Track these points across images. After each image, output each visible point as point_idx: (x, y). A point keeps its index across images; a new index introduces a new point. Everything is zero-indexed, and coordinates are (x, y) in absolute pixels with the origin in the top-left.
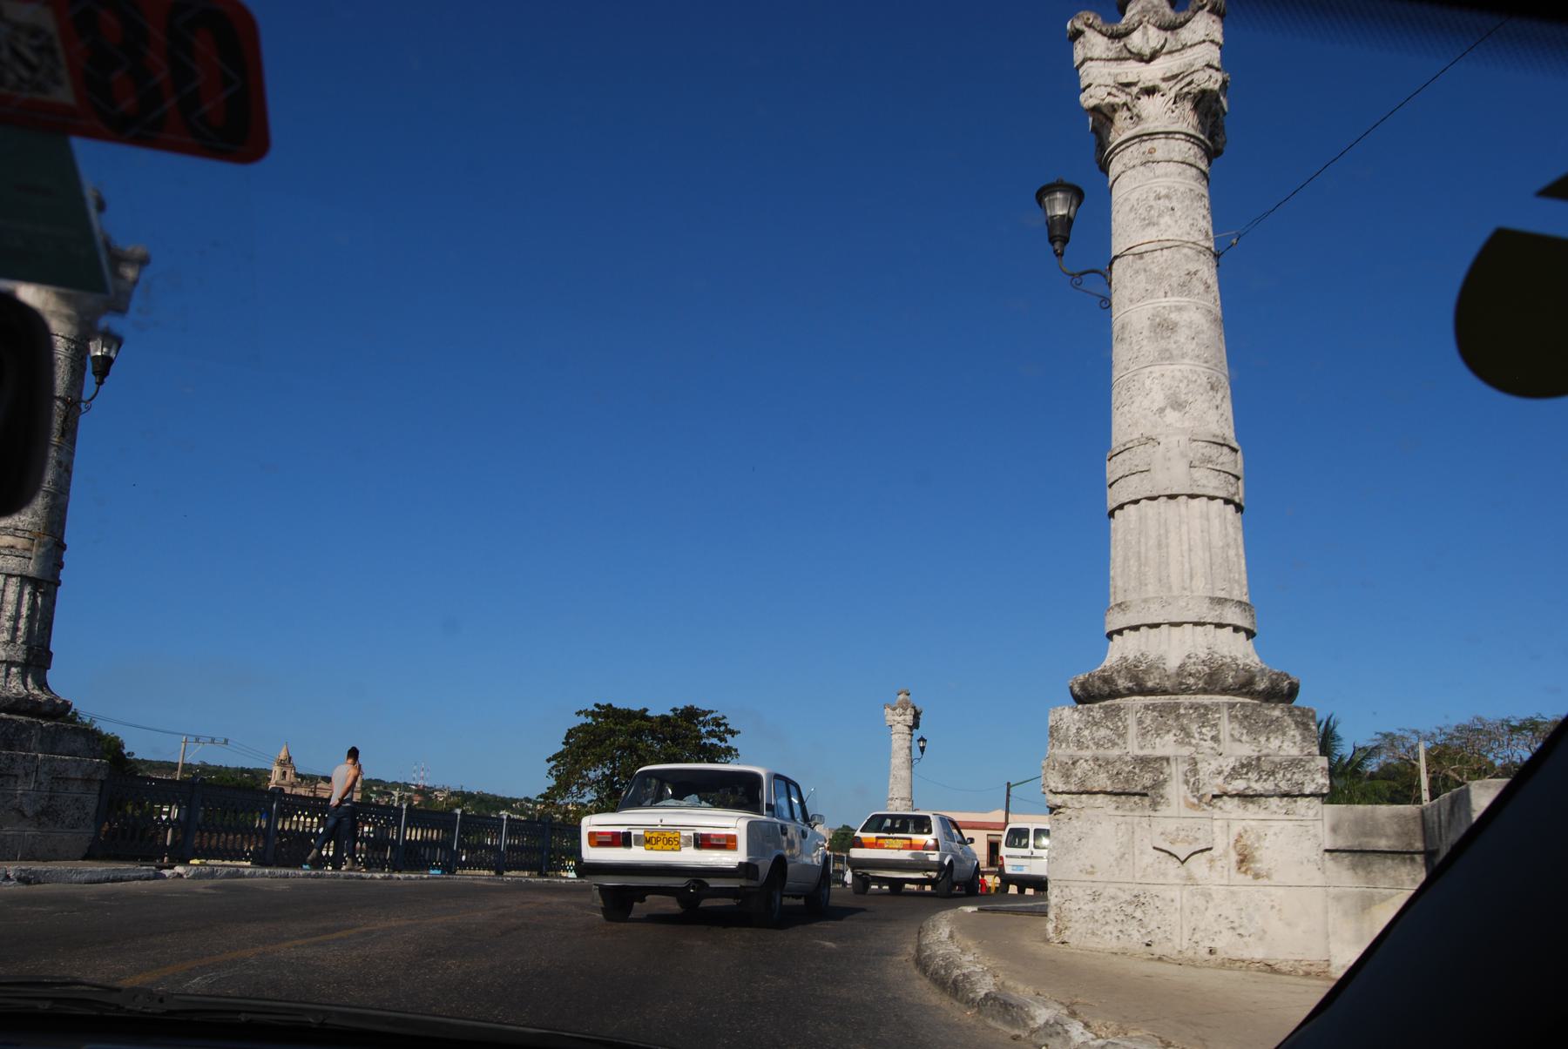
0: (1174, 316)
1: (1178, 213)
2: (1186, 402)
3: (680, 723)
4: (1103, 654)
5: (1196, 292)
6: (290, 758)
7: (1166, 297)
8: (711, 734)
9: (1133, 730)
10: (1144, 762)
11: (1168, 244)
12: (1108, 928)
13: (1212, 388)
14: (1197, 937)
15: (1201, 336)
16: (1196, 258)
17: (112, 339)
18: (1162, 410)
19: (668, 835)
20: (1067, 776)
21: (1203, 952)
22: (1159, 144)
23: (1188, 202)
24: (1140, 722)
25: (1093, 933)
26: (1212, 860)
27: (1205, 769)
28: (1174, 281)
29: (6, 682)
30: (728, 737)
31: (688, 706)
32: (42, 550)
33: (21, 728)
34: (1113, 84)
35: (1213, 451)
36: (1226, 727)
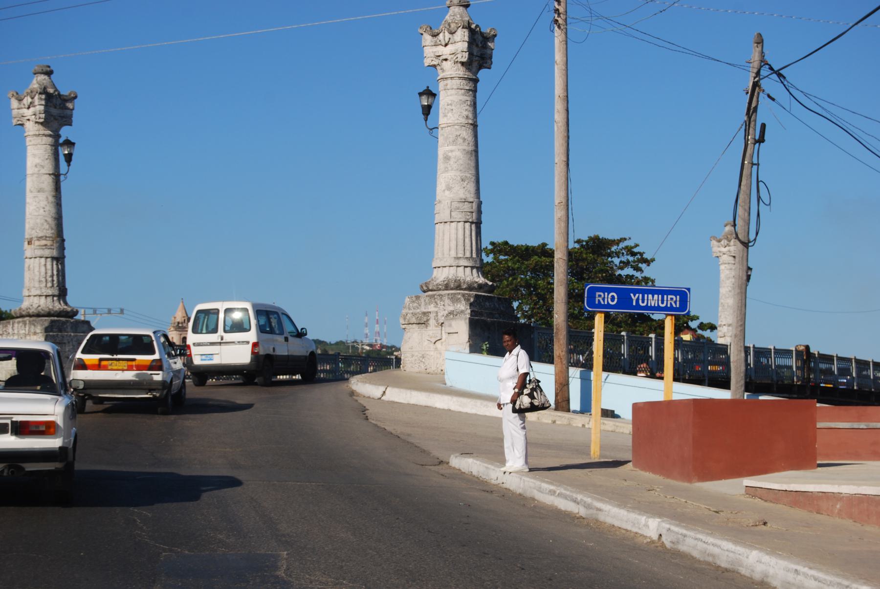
0: (450, 154)
1: (454, 111)
2: (452, 187)
3: (584, 256)
5: (459, 143)
7: (448, 146)
8: (626, 264)
9: (423, 303)
10: (424, 313)
11: (450, 125)
12: (416, 365)
13: (462, 180)
14: (438, 366)
15: (459, 161)
16: (460, 129)
17: (69, 143)
18: (444, 190)
20: (405, 319)
21: (439, 370)
22: (449, 81)
23: (458, 106)
24: (425, 301)
25: (412, 367)
26: (442, 343)
27: (440, 315)
28: (451, 140)
29: (53, 304)
30: (643, 266)
31: (592, 236)
32: (58, 244)
33: (64, 323)
34: (433, 56)
35: (461, 205)
36: (447, 301)
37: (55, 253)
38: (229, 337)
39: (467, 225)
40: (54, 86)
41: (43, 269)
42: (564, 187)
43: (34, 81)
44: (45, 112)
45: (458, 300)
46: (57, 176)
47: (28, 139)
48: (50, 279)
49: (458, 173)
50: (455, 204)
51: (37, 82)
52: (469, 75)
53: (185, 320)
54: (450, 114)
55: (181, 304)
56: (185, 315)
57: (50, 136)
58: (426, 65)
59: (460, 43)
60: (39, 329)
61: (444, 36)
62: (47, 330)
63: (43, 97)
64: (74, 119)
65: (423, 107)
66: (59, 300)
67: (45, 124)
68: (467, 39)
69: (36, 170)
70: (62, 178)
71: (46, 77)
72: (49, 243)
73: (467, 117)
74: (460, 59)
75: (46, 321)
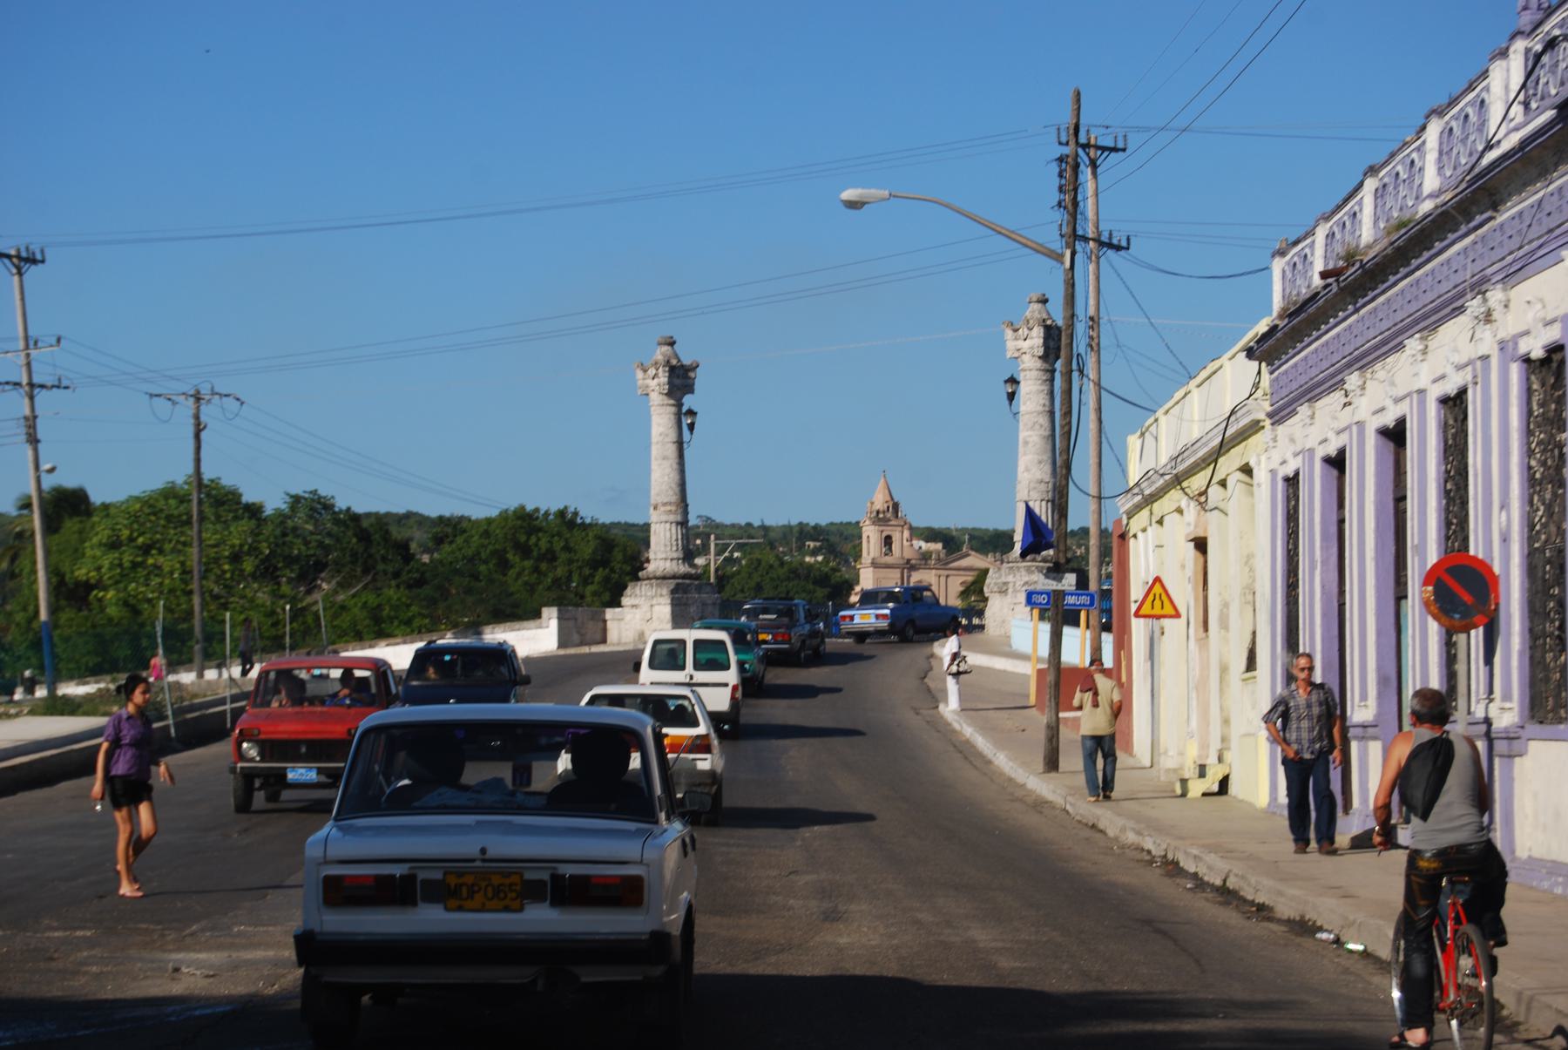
4: (555, 768)
6: (896, 506)
17: (691, 413)
19: (496, 880)
22: (1028, 372)
33: (689, 585)
37: (679, 518)
38: (702, 676)
39: (1044, 503)
40: (677, 356)
41: (668, 534)
42: (1096, 485)
43: (658, 352)
44: (670, 383)
45: (1032, 572)
46: (680, 444)
47: (652, 409)
48: (674, 543)
49: (1036, 457)
50: (1032, 485)
51: (661, 353)
52: (1046, 366)
53: (888, 507)
54: (1028, 403)
55: (882, 480)
56: (889, 499)
57: (673, 405)
58: (1008, 356)
59: (1036, 339)
60: (665, 591)
61: (1023, 331)
62: (673, 592)
63: (667, 369)
64: (697, 387)
65: (1008, 393)
66: (684, 563)
67: (669, 394)
68: (1042, 335)
69: (661, 438)
70: (685, 446)
71: (669, 348)
72: (673, 508)
73: (1044, 405)
74: (1036, 353)
75: (672, 583)
